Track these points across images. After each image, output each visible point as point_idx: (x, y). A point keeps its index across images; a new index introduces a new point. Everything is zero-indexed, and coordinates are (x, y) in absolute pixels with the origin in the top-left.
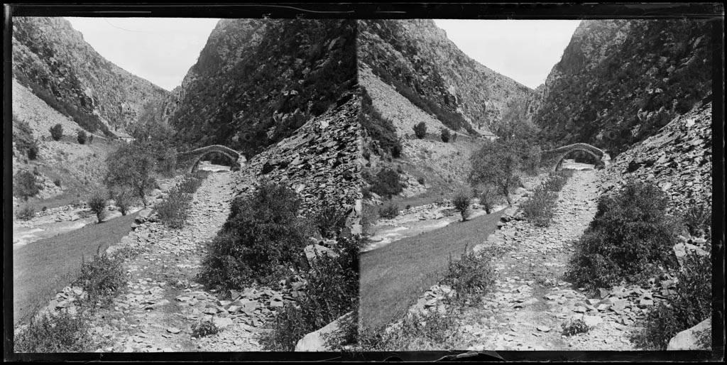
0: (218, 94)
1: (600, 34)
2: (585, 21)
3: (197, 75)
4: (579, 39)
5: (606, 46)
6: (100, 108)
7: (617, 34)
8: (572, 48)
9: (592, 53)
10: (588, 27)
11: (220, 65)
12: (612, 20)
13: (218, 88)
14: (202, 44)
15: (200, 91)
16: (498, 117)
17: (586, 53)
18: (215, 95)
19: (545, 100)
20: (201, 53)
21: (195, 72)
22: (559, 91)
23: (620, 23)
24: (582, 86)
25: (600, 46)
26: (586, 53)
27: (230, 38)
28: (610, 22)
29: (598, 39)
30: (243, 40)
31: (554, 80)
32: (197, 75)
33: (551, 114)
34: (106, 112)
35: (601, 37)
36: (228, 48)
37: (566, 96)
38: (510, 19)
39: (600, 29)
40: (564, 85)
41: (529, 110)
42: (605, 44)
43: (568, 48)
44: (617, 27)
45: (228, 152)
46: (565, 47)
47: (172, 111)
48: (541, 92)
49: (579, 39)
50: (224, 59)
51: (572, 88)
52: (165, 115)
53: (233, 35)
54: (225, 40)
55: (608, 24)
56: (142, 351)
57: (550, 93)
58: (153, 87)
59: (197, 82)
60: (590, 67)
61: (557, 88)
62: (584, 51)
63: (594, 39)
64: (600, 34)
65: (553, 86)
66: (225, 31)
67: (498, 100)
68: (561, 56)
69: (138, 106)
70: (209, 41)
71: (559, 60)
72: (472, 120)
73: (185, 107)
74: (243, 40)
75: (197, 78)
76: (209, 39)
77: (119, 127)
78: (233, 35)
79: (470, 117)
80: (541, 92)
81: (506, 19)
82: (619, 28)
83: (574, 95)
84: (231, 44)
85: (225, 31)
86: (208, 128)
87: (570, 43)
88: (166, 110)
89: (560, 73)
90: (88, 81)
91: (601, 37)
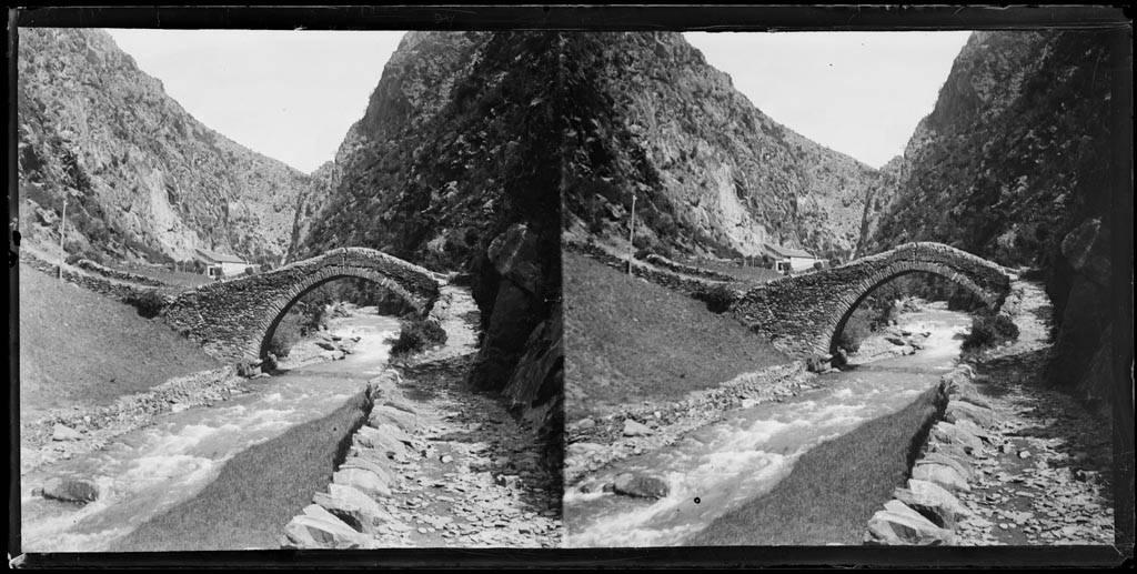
0: (973, 162)
1: (438, 58)
2: (976, 32)
3: (933, 133)
4: (397, 71)
5: (452, 80)
6: (750, 203)
7: (1041, 51)
8: (385, 94)
9: (425, 96)
10: (415, 49)
11: (408, 116)
12: (461, 33)
13: (973, 151)
14: (373, 80)
15: (938, 163)
16: (256, 230)
17: (982, 92)
18: (967, 164)
19: (336, 192)
20: (372, 98)
21: (361, 134)
22: (361, 173)
23: (478, 36)
24: (973, 151)
25: (439, 82)
26: (412, 97)
27: (997, 58)
28: (457, 37)
29: (434, 70)
30: (453, 66)
31: (920, 146)
32: (364, 138)
33: (343, 214)
34: (761, 209)
35: (1010, 60)
36: (424, 83)
37: (372, 178)
38: (332, 29)
39: (438, 51)
40: (370, 160)
41: (304, 211)
42: (1020, 71)
43: (377, 90)
44: (1042, 38)
45: (967, 269)
46: (373, 91)
47: (317, 208)
48: (327, 177)
49: (397, 71)
50: (416, 103)
51: (954, 157)
52: (303, 217)
53: (432, 57)
54: (416, 67)
55: (454, 40)
56: (954, 544)
57: (913, 172)
58: (292, 173)
59: (934, 145)
60: (990, 115)
61: (358, 167)
62: (407, 94)
63: (996, 63)
64: (438, 58)
65: (349, 165)
66: (986, 46)
67: (256, 200)
68: (934, 103)
69: (262, 207)
70: (385, 74)
71: (361, 116)
72: (198, 233)
73: (910, 193)
74: (453, 66)
75: (363, 143)
76: (955, 61)
77: (787, 238)
78: (432, 57)
79: (193, 229)
80: (327, 177)
81: (766, 31)
82: (476, 47)
83: (958, 169)
84: (998, 69)
85: (986, 46)
86: (950, 227)
87: (950, 76)
88: (873, 201)
89: (364, 138)
90: (724, 152)
91: (1010, 60)
